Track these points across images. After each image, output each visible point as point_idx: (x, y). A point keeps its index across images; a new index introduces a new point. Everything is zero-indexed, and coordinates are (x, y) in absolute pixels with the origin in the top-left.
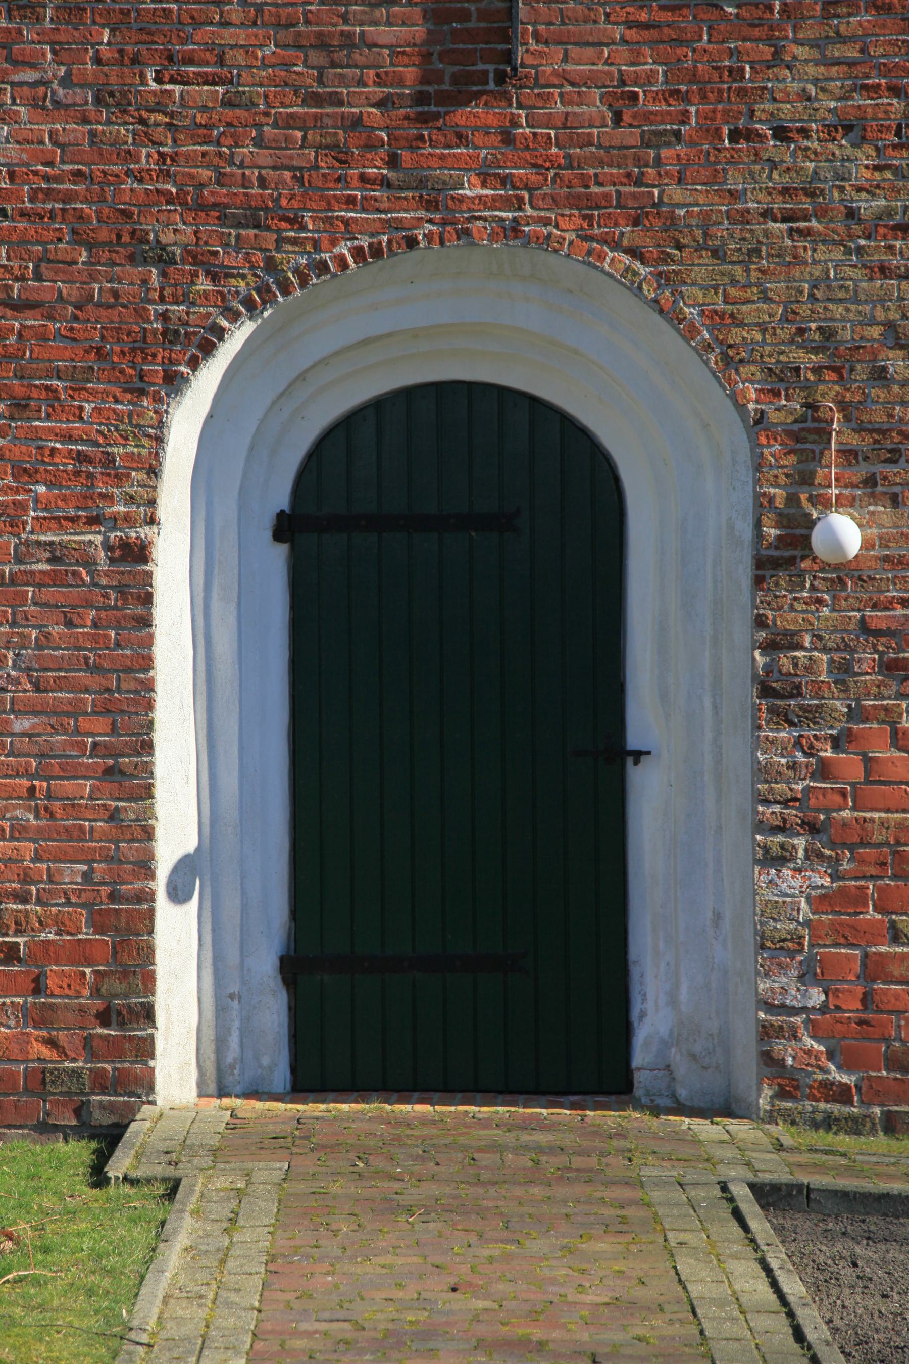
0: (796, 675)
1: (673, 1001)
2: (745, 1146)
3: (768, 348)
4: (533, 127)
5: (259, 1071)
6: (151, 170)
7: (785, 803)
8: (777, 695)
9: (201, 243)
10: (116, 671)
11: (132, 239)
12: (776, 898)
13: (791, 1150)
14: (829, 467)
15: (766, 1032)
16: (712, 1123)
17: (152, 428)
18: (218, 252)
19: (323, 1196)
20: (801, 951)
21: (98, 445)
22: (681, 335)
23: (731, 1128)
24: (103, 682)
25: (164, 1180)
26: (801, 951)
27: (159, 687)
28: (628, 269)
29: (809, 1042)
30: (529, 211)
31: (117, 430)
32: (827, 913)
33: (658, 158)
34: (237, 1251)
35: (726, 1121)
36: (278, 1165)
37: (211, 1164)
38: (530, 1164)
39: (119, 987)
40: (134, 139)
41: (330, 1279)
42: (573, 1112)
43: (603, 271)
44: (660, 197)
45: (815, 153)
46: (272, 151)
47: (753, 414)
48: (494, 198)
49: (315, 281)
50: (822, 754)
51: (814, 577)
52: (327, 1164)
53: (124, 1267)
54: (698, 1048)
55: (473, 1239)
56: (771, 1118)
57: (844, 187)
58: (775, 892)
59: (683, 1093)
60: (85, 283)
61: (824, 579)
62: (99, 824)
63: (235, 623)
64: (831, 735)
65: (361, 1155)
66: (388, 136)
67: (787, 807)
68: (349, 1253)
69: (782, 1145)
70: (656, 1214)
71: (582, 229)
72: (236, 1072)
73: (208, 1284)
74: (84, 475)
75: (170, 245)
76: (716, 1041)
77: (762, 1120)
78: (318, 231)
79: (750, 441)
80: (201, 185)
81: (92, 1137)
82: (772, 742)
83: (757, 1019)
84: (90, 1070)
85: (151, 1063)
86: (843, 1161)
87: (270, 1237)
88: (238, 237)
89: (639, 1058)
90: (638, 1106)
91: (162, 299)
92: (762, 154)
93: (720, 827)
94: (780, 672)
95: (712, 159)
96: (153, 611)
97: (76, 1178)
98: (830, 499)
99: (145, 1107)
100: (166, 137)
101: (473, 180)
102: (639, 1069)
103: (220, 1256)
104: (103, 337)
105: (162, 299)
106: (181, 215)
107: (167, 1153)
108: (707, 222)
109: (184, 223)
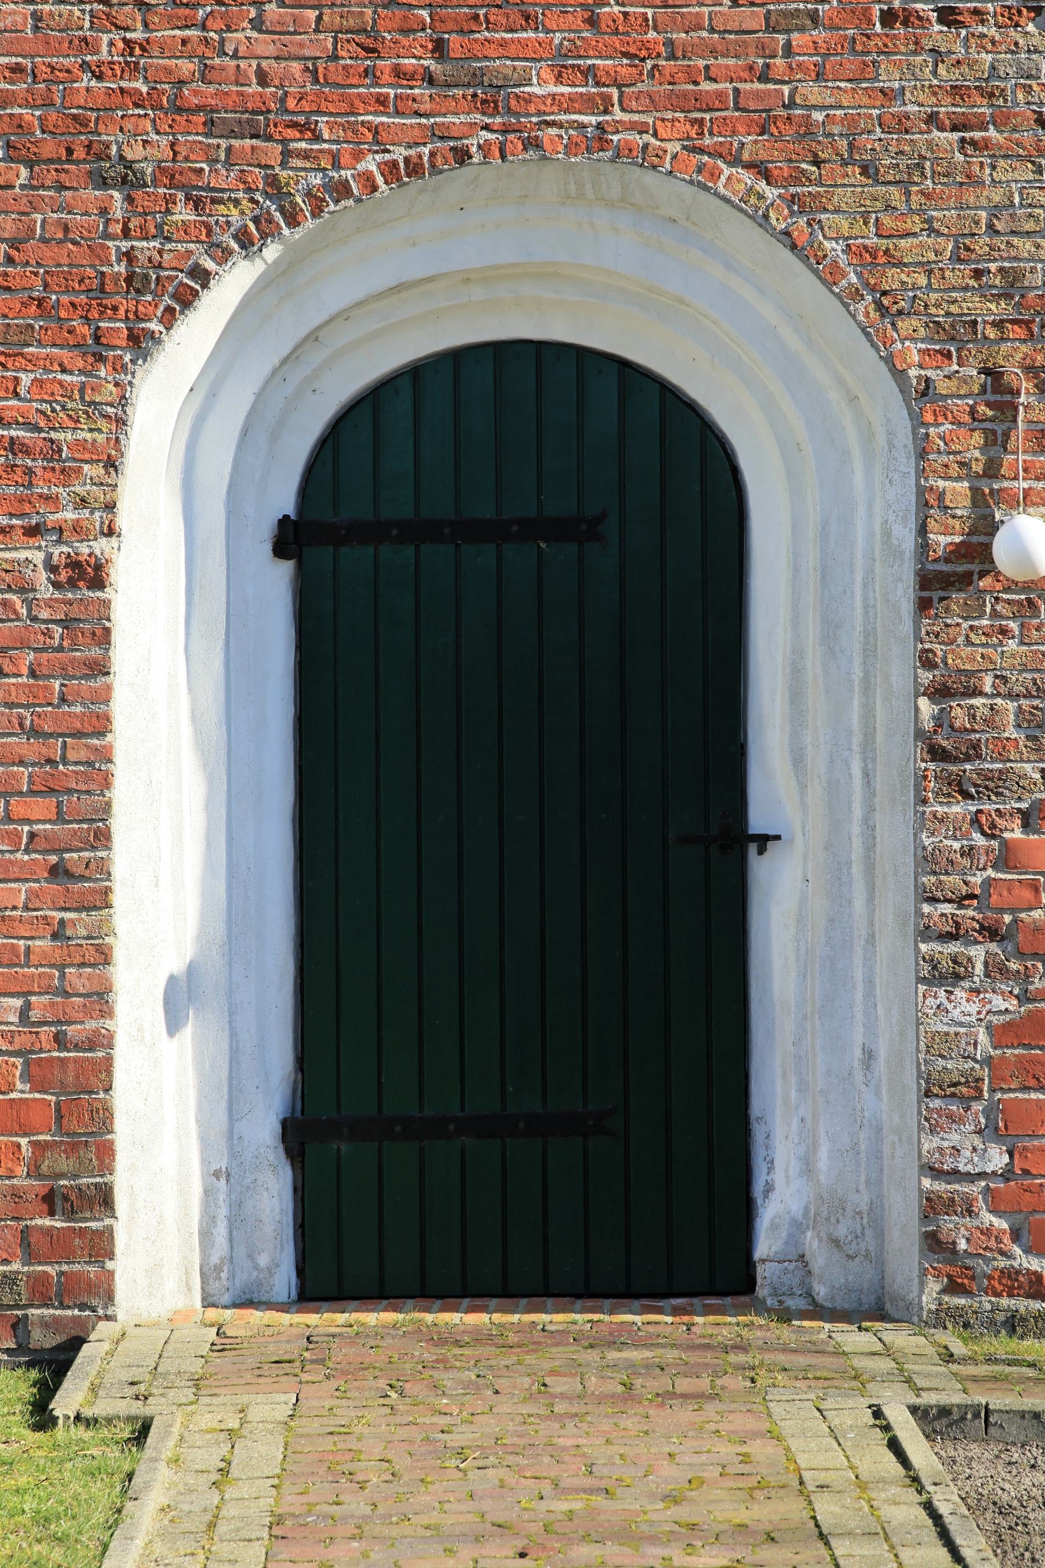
0: (974, 731)
1: (808, 1169)
2: (911, 1362)
3: (934, 296)
4: (623, 5)
5: (255, 1273)
6: (113, 63)
7: (960, 901)
8: (949, 755)
9: (180, 158)
10: (61, 735)
11: (88, 154)
12: (946, 1029)
13: (963, 1360)
14: (1016, 453)
15: (932, 1207)
16: (860, 1328)
17: (112, 406)
18: (202, 170)
19: (342, 1437)
20: (979, 1097)
21: (38, 429)
22: (820, 278)
23: (887, 1337)
24: (44, 750)
25: (130, 1419)
26: (979, 1097)
27: (119, 756)
28: (750, 190)
29: (988, 1218)
30: (618, 115)
31: (64, 408)
32: (1013, 1047)
33: (788, 45)
34: (230, 1511)
35: (878, 1325)
36: (282, 1398)
37: (192, 1398)
38: (620, 1389)
39: (65, 1164)
40: (92, 22)
41: (355, 1544)
42: (677, 1319)
43: (716, 194)
44: (792, 96)
45: (993, 42)
46: (277, 37)
47: (914, 382)
48: (571, 98)
49: (332, 207)
50: (1007, 835)
51: (997, 599)
52: (348, 1395)
53: (80, 1533)
54: (841, 1231)
55: (546, 1488)
56: (940, 1318)
57: (1030, 86)
58: (945, 1020)
59: (821, 1291)
60: (23, 214)
61: (1009, 602)
62: (38, 943)
63: (222, 670)
64: (1019, 810)
65: (394, 1382)
66: (431, 16)
67: (961, 906)
68: (381, 1510)
69: (952, 1355)
70: (788, 1449)
71: (688, 138)
72: (224, 1275)
73: (193, 1554)
74: (19, 471)
75: (139, 161)
76: (865, 1220)
77: (926, 1323)
78: (337, 142)
79: (911, 419)
80: (180, 82)
81: (30, 1365)
82: (941, 821)
83: (920, 1190)
84: (28, 1275)
85: (109, 1265)
86: (1030, 1372)
87: (274, 1492)
88: (229, 150)
89: (766, 1244)
90: (760, 1308)
91: (126, 233)
92: (924, 41)
93: (873, 936)
94: (952, 727)
95: (859, 48)
96: (111, 654)
97: (12, 1418)
98: (1017, 495)
99: (102, 1325)
100: (134, 20)
101: (543, 73)
102: (764, 1261)
103: (208, 1517)
104: (46, 285)
105: (126, 233)
106: (154, 121)
107: (132, 1384)
108: (853, 130)
109: (158, 133)
